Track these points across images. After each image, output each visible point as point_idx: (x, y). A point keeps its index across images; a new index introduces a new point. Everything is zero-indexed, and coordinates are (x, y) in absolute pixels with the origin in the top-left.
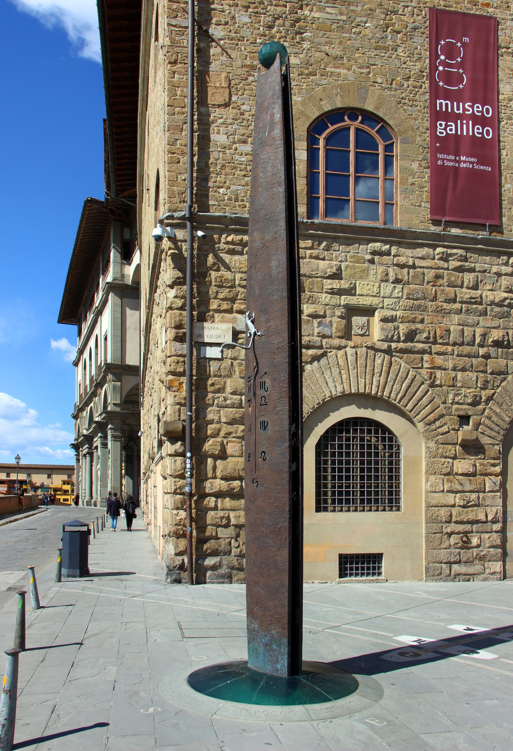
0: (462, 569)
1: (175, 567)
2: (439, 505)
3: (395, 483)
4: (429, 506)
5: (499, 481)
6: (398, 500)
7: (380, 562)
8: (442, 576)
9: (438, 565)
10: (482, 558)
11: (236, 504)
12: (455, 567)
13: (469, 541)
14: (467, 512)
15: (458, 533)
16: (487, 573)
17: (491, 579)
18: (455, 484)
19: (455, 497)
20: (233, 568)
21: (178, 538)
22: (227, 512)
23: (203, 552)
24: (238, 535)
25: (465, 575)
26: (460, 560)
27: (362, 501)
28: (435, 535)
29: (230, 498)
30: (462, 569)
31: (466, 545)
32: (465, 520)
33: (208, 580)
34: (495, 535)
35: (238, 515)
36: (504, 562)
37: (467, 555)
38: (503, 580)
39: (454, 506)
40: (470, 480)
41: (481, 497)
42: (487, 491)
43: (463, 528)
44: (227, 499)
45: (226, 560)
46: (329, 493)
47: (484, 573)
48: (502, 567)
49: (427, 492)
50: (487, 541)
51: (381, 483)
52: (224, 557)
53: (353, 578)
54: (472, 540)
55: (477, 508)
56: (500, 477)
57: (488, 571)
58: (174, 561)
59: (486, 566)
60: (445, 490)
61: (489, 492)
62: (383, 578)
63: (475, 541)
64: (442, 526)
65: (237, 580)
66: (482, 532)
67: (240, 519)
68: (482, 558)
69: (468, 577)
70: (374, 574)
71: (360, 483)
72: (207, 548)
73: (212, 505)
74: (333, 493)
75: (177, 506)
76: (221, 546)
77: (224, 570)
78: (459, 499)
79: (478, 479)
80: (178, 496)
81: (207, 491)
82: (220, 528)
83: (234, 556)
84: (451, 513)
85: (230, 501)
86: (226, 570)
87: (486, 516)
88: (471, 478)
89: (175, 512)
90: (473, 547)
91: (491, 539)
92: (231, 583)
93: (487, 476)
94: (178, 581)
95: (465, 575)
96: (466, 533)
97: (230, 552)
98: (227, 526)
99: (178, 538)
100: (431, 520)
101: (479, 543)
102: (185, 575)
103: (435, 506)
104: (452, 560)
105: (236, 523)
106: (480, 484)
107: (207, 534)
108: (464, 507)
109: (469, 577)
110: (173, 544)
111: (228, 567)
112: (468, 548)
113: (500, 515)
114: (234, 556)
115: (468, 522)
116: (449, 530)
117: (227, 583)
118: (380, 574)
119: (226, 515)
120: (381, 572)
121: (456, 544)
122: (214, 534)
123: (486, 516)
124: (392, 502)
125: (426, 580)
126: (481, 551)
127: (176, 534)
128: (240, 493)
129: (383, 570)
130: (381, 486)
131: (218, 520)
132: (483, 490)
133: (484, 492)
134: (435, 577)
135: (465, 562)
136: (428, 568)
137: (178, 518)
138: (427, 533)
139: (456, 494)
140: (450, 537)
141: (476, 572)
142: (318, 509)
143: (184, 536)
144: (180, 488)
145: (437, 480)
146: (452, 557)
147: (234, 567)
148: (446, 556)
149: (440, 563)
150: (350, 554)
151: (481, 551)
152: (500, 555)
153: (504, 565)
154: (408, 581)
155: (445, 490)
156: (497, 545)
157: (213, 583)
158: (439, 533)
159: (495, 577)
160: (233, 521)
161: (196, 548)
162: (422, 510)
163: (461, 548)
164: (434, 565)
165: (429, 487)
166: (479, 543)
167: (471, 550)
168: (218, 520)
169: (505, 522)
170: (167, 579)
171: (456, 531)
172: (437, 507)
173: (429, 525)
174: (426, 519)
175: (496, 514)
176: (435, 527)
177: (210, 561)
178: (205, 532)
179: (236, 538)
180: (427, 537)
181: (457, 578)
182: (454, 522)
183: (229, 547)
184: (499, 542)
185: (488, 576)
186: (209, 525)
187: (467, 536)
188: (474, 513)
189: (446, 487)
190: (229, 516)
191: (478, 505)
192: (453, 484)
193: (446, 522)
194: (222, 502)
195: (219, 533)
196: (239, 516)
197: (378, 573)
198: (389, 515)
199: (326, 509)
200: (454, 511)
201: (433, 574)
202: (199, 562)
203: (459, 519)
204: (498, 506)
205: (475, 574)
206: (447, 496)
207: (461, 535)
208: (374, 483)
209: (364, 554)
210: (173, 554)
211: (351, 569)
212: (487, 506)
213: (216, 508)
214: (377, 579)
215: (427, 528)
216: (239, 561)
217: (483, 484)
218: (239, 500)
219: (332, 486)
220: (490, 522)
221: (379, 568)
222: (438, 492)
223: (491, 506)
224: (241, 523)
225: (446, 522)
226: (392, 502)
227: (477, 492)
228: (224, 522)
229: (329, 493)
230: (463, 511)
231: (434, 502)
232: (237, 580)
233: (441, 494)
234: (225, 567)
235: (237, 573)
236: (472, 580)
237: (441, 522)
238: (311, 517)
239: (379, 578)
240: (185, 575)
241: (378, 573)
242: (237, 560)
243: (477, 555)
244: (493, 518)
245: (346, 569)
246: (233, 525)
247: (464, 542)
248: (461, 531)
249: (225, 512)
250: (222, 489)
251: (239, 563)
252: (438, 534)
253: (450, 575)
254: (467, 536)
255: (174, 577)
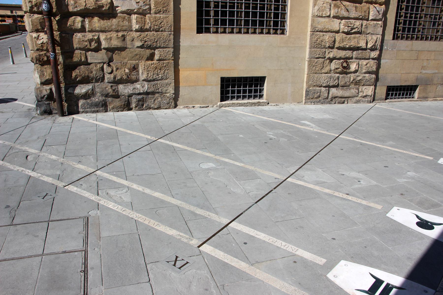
0: (339, 92)
1: (42, 98)
2: (324, 30)
3: (282, 5)
4: (314, 31)
5: (383, 10)
6: (283, 23)
7: (262, 85)
8: (320, 99)
9: (318, 88)
10: (357, 83)
11: (106, 25)
12: (333, 91)
13: (348, 67)
14: (349, 39)
15: (340, 59)
16: (360, 96)
17: (362, 101)
18: (342, 9)
19: (340, 23)
20: (107, 96)
21: (42, 65)
22: (97, 33)
23: (73, 80)
24: (111, 60)
25: (341, 98)
26: (338, 84)
27: (247, 23)
28: (318, 60)
29: (99, 18)
30: (339, 92)
31: (345, 70)
32: (347, 46)
33: (81, 110)
34: (372, 62)
35: (109, 37)
36: (375, 86)
37: (345, 80)
38: (373, 101)
39: (338, 32)
40: (356, 7)
41: (364, 25)
42: (370, 19)
43: (344, 54)
44: (96, 19)
45: (99, 87)
46: (212, 13)
47: (357, 96)
48: (373, 91)
49: (313, 16)
50: (364, 68)
51: (267, 4)
52: (97, 84)
53: (235, 101)
54: (351, 66)
55: (359, 35)
56: (384, 6)
57: (361, 94)
58: (41, 91)
59: (360, 90)
60: (332, 16)
61: (372, 20)
62: (265, 101)
63: (353, 67)
64: (325, 52)
65: (113, 108)
66: (360, 59)
67: (112, 42)
68: (357, 83)
69: (343, 100)
70: (255, 97)
71: (245, 3)
72: (76, 75)
73: (79, 26)
74: (216, 13)
75: (36, 28)
76: (92, 72)
77: (97, 98)
78: (345, 25)
79: (364, 6)
80: (36, 16)
81: (71, 9)
82: (90, 52)
83: (108, 82)
84: (335, 39)
85: (99, 21)
86: (101, 98)
87: (367, 43)
88: (357, 5)
89: (35, 35)
90: (351, 73)
91: (368, 65)
92: (106, 111)
93: (372, 4)
94: (48, 112)
95: (341, 98)
96: (346, 59)
97: (103, 79)
98: (97, 49)
99: (42, 65)
100: (315, 45)
101: (357, 68)
102: (54, 105)
103: (320, 31)
104: (331, 84)
105: (107, 46)
106: (365, 12)
107: (75, 59)
108: (348, 33)
109: (344, 99)
110: (38, 72)
111: (102, 95)
112: (347, 73)
113: (379, 43)
114: (108, 82)
115: (350, 49)
116: (331, 56)
117: (102, 112)
118: (261, 96)
119: (96, 38)
120: (263, 95)
121: (337, 69)
122: (83, 59)
123: (367, 43)
124: (277, 25)
125: (305, 103)
126: (358, 76)
127: (40, 61)
128: (111, 12)
129: (265, 92)
130: (267, 7)
131: (86, 43)
132: (367, 18)
133: (367, 20)
134: (314, 100)
135: (343, 86)
136: (308, 91)
137: (40, 42)
138: (310, 58)
139: (342, 20)
140: (331, 62)
141: (351, 95)
142: (199, 31)
143: (48, 62)
144: (36, 5)
145: (325, 5)
146: (331, 82)
147: (108, 94)
148: (326, 81)
149: (320, 87)
150: (232, 78)
151: (358, 76)
152: (373, 80)
153: (375, 89)
154: (288, 104)
155: (332, 16)
156: (373, 71)
157: (87, 112)
158: (322, 58)
159: (366, 99)
160: (104, 44)
161: (64, 76)
162: (306, 35)
163: (340, 73)
164: (314, 88)
165: (316, 10)
166: (357, 68)
167: (349, 75)
168: (86, 43)
169: (381, 50)
170: (37, 110)
171: (338, 57)
172: (322, 32)
173: (313, 49)
174: (311, 44)
175: (376, 42)
176: (319, 52)
177: (81, 90)
178: (72, 57)
179: (108, 63)
180: (310, 62)
181: (334, 101)
182: (337, 48)
183: (101, 73)
184: (374, 69)
185: (361, 98)
186: (77, 49)
187: (347, 62)
188: (356, 40)
189: (333, 13)
190: (99, 38)
191: (359, 33)
192: (340, 10)
193: (329, 47)
194: (90, 22)
195: (89, 58)
196: (111, 39)
197: (260, 95)
198: (273, 39)
199: (208, 31)
200: (338, 37)
201: (313, 97)
202: (69, 91)
203: (341, 45)
204: (378, 34)
205: (350, 97)
206: (333, 21)
207: (342, 61)
208: (260, 4)
209: (247, 77)
210: (39, 83)
211: (233, 92)
212: (369, 34)
213: (83, 30)
214: (259, 102)
215: (310, 53)
216: (114, 88)
217: (367, 12)
218: (109, 19)
219: (215, 5)
220: (369, 49)
221: (261, 91)
222: (325, 17)
223: (372, 34)
224: (113, 46)
225: (329, 47)
226: (277, 25)
227: (361, 19)
228: (94, 45)
229: (212, 13)
230: (346, 37)
231: (320, 27)
232: (113, 108)
233: (327, 19)
234: (98, 94)
235: (112, 101)
236: (346, 103)
237: (325, 47)
238: (190, 38)
239: (261, 101)
240: (54, 105)
241: (260, 95)
242: (112, 86)
243: (354, 80)
244: (373, 46)
245: (228, 92)
246: (104, 49)
247: (344, 67)
248: (342, 57)
249: (94, 34)
250: (88, 6)
251: (114, 90)
252: (320, 59)
253: (327, 98)
254: (347, 62)
255: (43, 109)
